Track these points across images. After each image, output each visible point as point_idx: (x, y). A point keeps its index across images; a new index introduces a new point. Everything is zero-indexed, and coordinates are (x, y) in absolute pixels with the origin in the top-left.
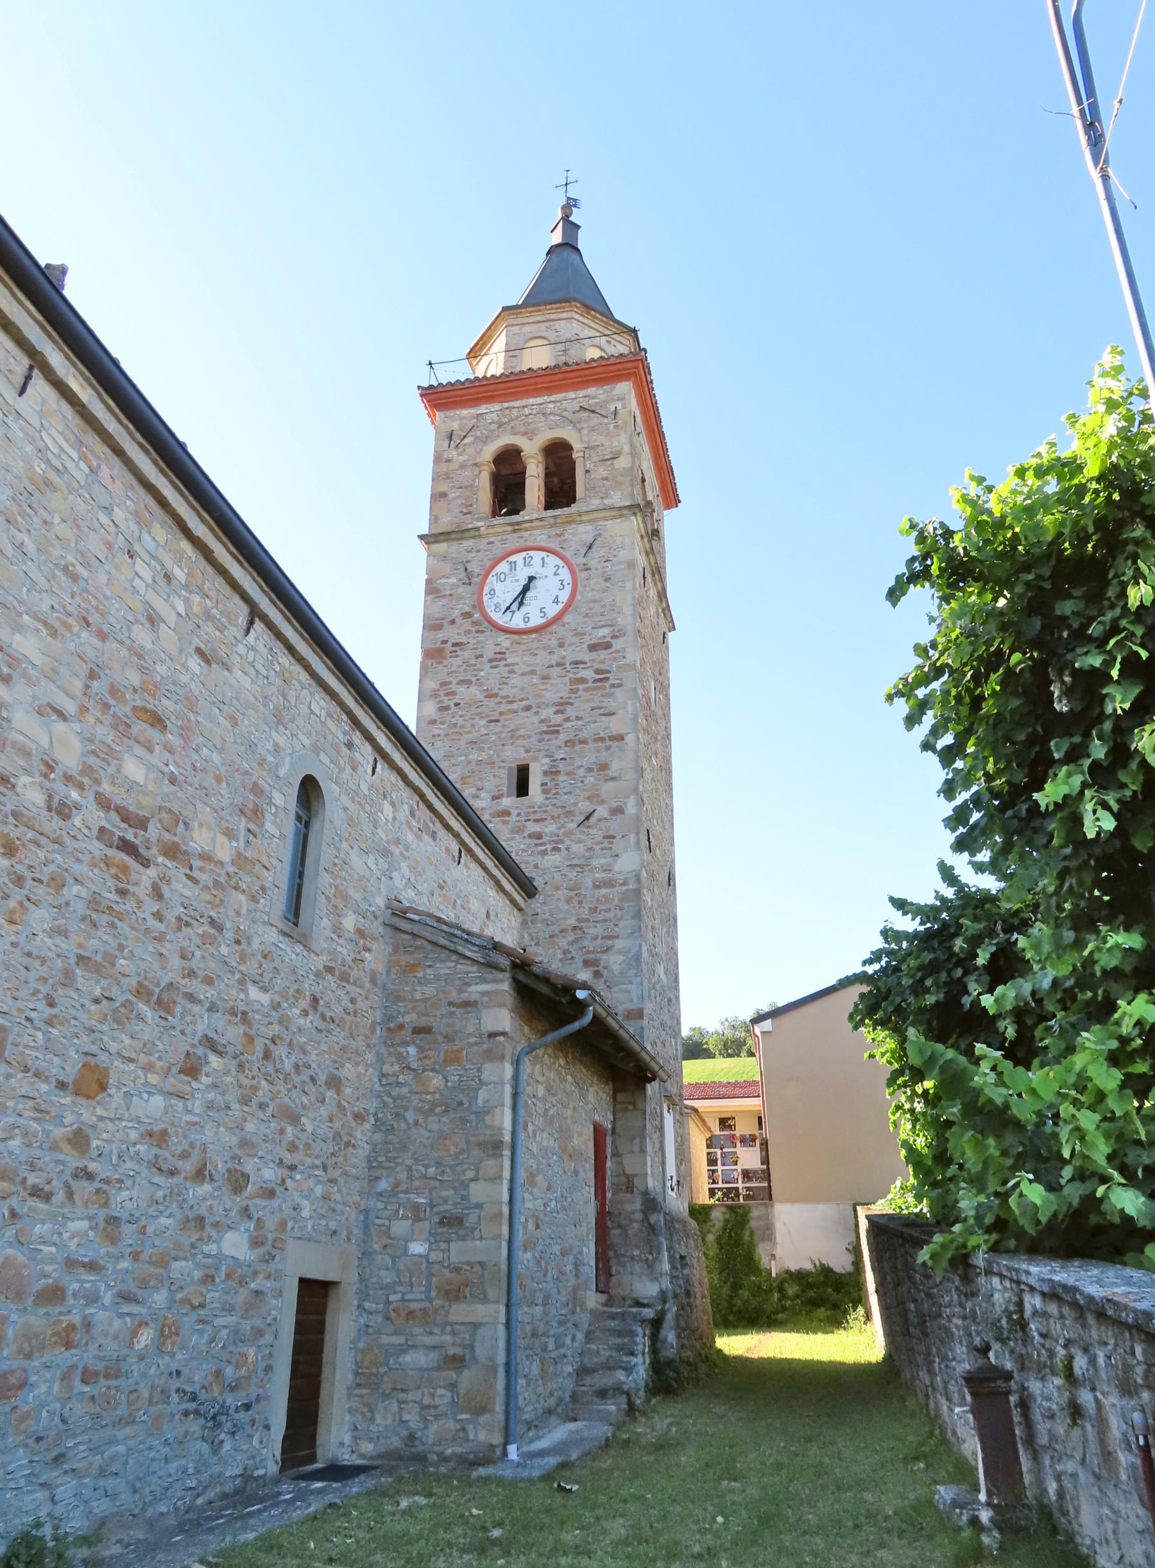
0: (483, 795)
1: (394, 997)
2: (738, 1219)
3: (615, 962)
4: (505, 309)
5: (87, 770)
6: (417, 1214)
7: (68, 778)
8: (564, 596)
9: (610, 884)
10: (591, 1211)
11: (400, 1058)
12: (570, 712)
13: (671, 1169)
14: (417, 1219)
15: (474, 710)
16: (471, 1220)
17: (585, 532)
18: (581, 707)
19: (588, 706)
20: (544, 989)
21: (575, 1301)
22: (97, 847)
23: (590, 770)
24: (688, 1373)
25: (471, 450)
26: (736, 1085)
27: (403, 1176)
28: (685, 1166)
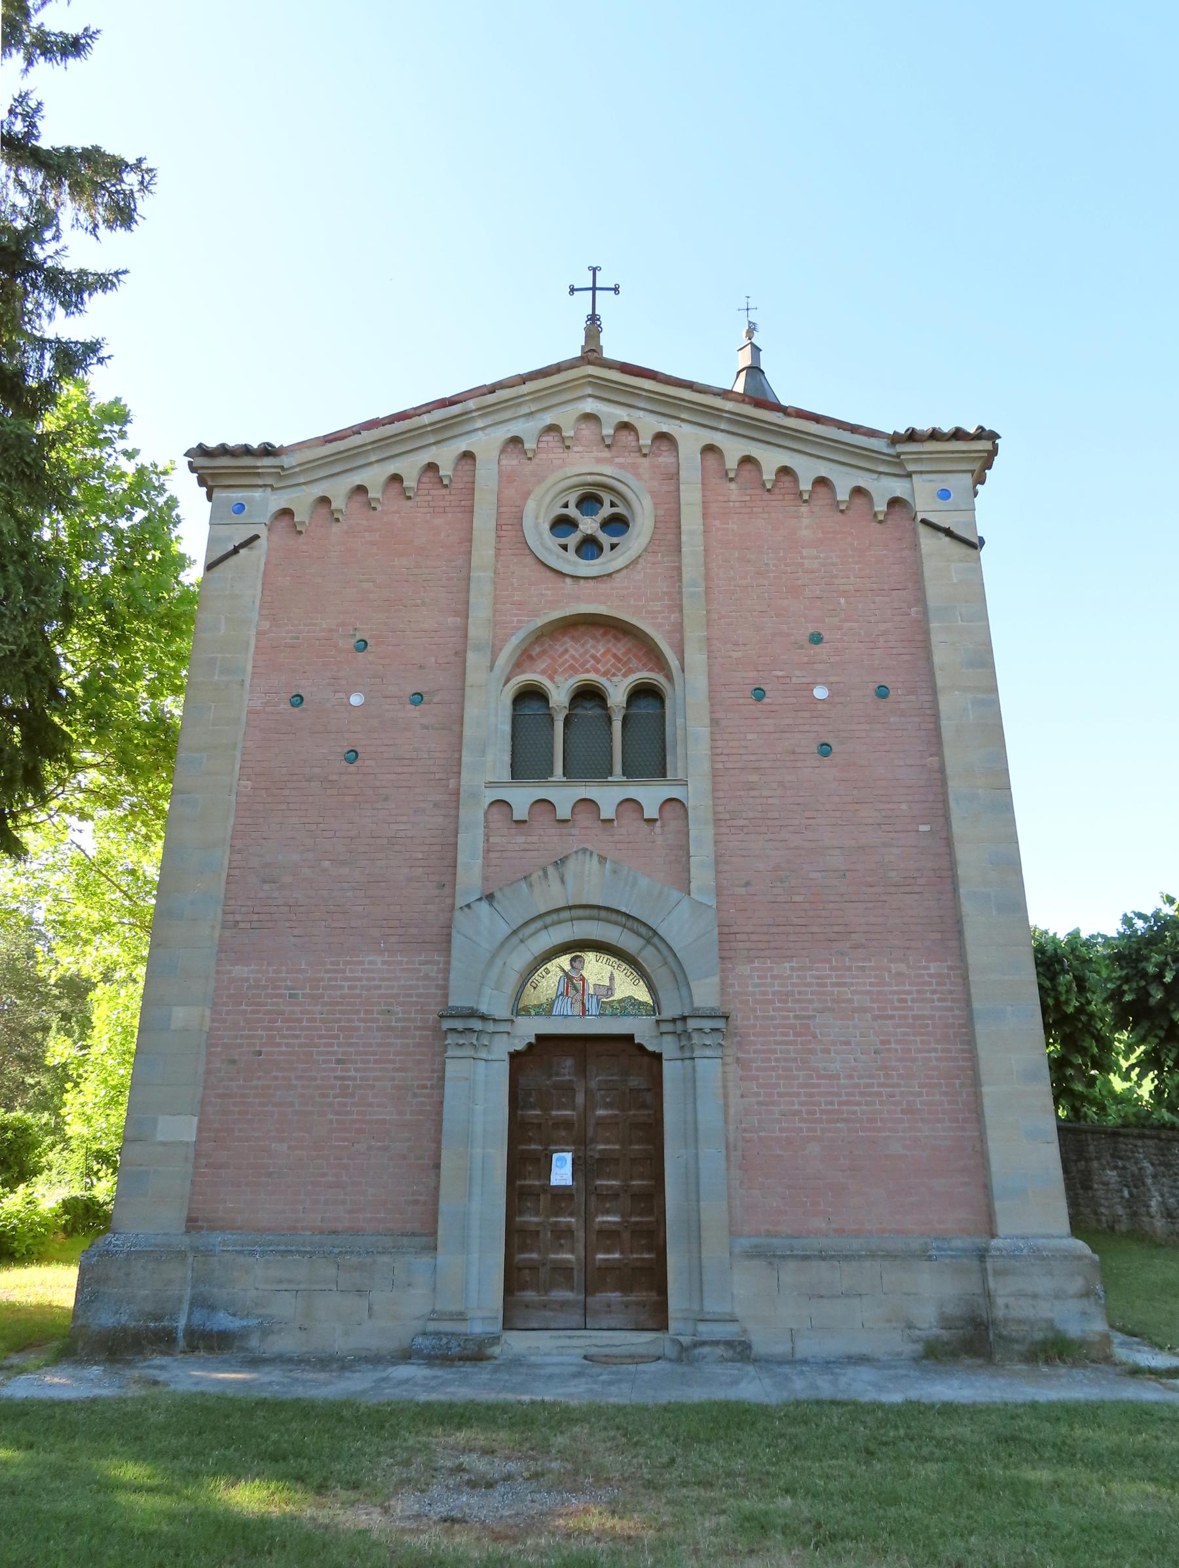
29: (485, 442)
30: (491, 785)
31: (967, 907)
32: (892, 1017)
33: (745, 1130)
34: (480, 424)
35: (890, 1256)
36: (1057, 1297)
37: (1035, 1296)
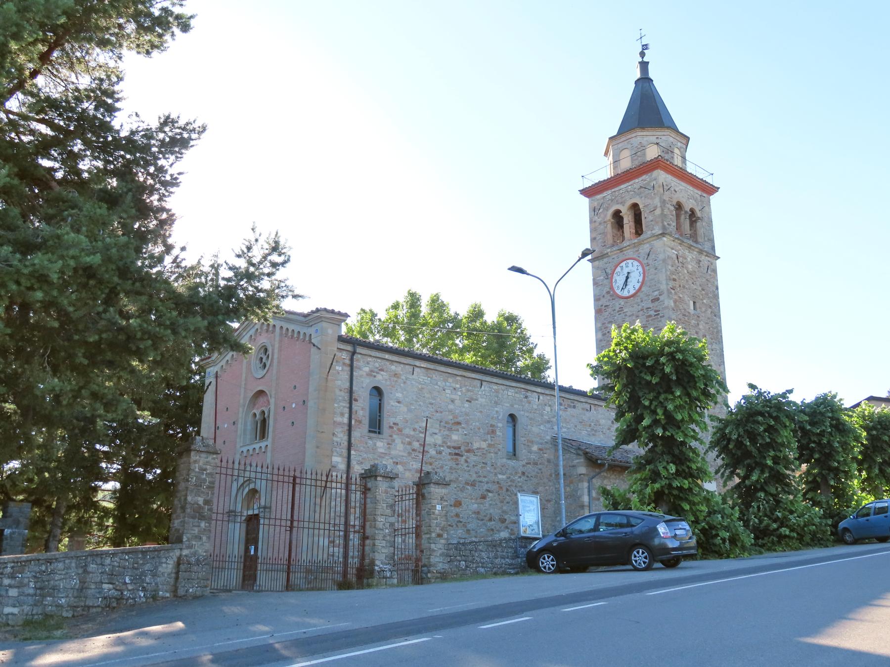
4: (611, 138)
5: (444, 442)
7: (440, 446)
22: (449, 457)
25: (602, 215)
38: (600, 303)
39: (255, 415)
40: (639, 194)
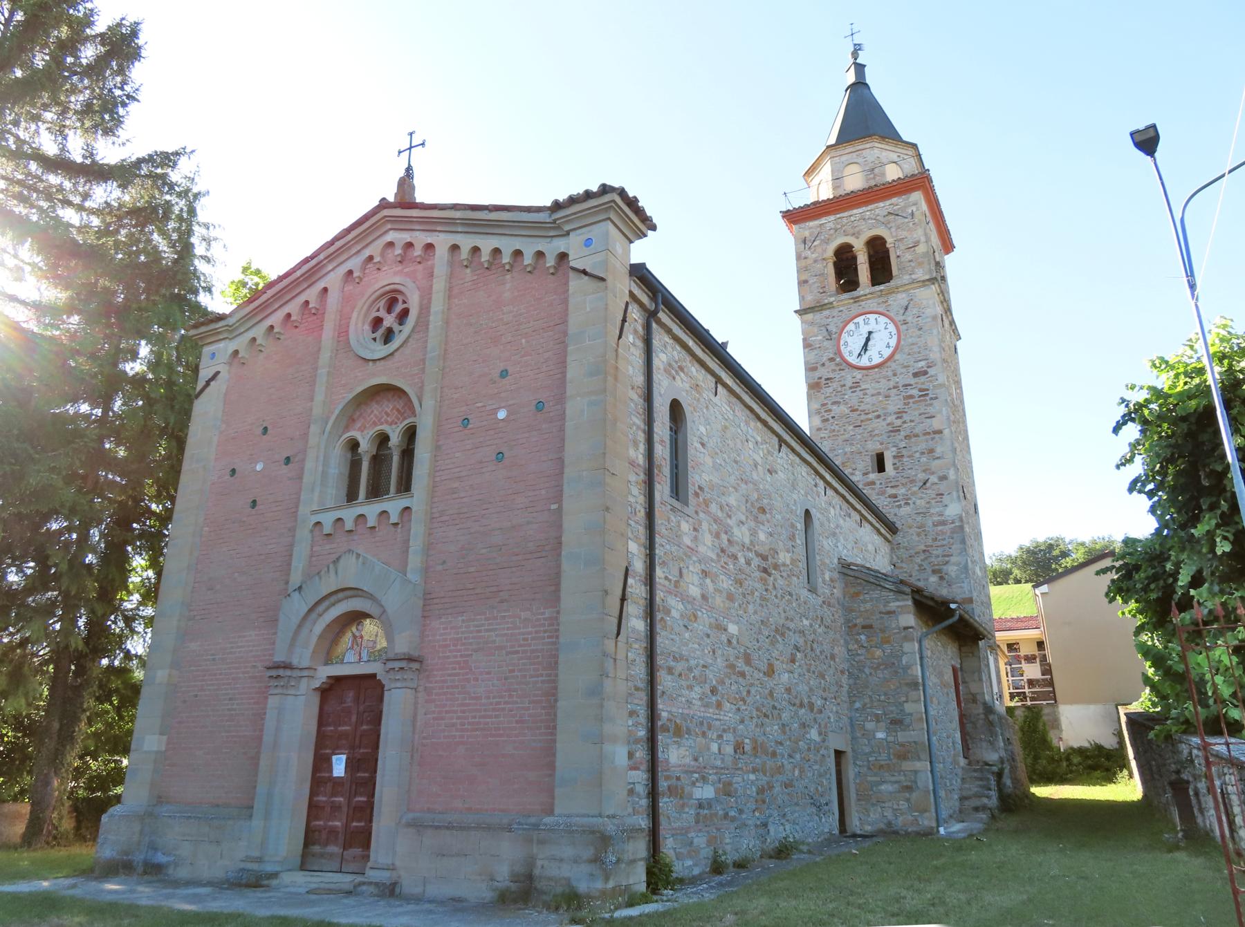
0: (857, 473)
1: (849, 610)
2: (1033, 715)
3: (952, 570)
4: (828, 147)
6: (878, 719)
8: (893, 342)
9: (943, 523)
10: (956, 714)
11: (857, 641)
12: (906, 417)
13: (996, 690)
14: (878, 721)
15: (844, 420)
16: (907, 721)
17: (902, 298)
18: (913, 413)
19: (917, 413)
20: (931, 603)
21: (955, 762)
23: (923, 453)
24: (1014, 806)
25: (819, 250)
26: (1018, 620)
27: (867, 700)
28: (1003, 683)
29: (333, 279)
30: (314, 512)
31: (565, 566)
32: (517, 652)
33: (424, 738)
34: (330, 267)
35: (489, 828)
36: (575, 862)
37: (561, 860)
38: (817, 374)
39: (354, 445)
40: (885, 224)
